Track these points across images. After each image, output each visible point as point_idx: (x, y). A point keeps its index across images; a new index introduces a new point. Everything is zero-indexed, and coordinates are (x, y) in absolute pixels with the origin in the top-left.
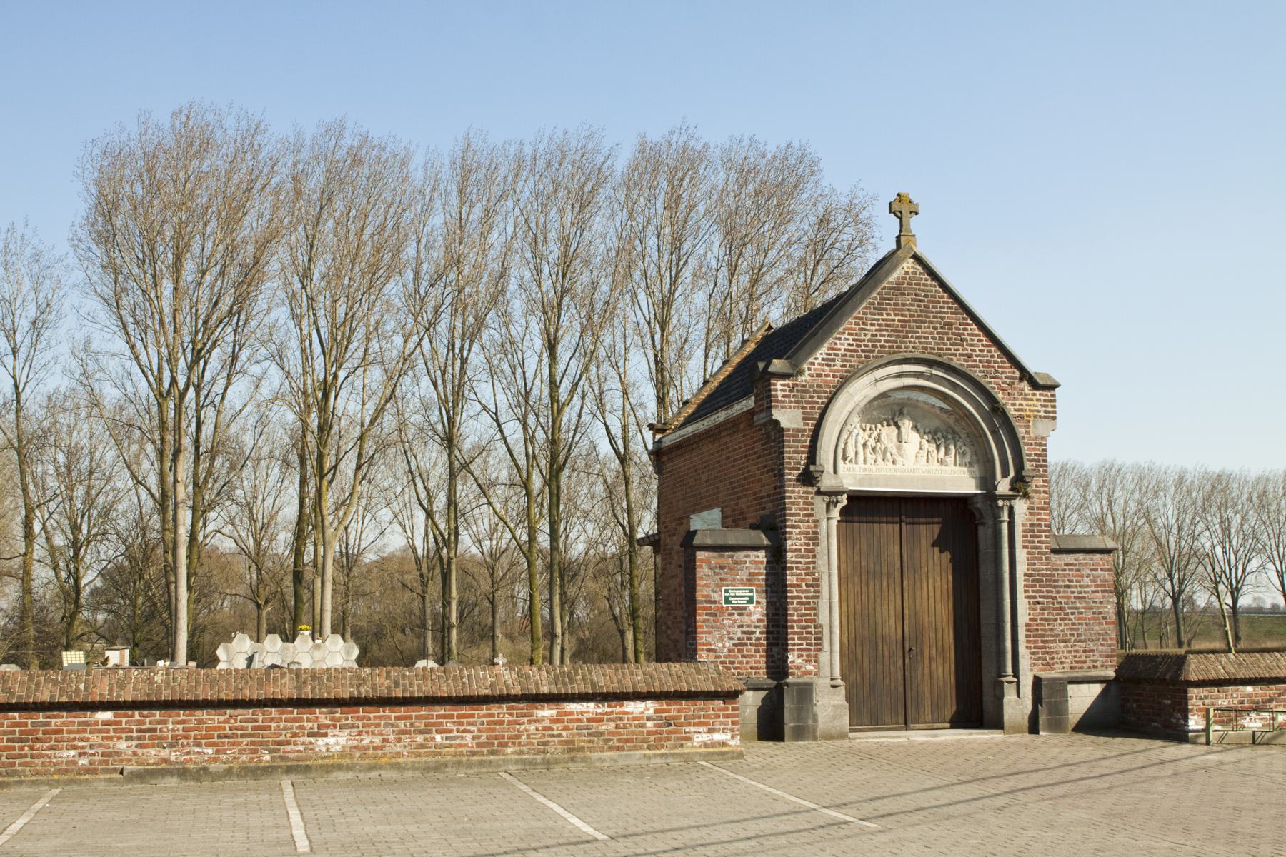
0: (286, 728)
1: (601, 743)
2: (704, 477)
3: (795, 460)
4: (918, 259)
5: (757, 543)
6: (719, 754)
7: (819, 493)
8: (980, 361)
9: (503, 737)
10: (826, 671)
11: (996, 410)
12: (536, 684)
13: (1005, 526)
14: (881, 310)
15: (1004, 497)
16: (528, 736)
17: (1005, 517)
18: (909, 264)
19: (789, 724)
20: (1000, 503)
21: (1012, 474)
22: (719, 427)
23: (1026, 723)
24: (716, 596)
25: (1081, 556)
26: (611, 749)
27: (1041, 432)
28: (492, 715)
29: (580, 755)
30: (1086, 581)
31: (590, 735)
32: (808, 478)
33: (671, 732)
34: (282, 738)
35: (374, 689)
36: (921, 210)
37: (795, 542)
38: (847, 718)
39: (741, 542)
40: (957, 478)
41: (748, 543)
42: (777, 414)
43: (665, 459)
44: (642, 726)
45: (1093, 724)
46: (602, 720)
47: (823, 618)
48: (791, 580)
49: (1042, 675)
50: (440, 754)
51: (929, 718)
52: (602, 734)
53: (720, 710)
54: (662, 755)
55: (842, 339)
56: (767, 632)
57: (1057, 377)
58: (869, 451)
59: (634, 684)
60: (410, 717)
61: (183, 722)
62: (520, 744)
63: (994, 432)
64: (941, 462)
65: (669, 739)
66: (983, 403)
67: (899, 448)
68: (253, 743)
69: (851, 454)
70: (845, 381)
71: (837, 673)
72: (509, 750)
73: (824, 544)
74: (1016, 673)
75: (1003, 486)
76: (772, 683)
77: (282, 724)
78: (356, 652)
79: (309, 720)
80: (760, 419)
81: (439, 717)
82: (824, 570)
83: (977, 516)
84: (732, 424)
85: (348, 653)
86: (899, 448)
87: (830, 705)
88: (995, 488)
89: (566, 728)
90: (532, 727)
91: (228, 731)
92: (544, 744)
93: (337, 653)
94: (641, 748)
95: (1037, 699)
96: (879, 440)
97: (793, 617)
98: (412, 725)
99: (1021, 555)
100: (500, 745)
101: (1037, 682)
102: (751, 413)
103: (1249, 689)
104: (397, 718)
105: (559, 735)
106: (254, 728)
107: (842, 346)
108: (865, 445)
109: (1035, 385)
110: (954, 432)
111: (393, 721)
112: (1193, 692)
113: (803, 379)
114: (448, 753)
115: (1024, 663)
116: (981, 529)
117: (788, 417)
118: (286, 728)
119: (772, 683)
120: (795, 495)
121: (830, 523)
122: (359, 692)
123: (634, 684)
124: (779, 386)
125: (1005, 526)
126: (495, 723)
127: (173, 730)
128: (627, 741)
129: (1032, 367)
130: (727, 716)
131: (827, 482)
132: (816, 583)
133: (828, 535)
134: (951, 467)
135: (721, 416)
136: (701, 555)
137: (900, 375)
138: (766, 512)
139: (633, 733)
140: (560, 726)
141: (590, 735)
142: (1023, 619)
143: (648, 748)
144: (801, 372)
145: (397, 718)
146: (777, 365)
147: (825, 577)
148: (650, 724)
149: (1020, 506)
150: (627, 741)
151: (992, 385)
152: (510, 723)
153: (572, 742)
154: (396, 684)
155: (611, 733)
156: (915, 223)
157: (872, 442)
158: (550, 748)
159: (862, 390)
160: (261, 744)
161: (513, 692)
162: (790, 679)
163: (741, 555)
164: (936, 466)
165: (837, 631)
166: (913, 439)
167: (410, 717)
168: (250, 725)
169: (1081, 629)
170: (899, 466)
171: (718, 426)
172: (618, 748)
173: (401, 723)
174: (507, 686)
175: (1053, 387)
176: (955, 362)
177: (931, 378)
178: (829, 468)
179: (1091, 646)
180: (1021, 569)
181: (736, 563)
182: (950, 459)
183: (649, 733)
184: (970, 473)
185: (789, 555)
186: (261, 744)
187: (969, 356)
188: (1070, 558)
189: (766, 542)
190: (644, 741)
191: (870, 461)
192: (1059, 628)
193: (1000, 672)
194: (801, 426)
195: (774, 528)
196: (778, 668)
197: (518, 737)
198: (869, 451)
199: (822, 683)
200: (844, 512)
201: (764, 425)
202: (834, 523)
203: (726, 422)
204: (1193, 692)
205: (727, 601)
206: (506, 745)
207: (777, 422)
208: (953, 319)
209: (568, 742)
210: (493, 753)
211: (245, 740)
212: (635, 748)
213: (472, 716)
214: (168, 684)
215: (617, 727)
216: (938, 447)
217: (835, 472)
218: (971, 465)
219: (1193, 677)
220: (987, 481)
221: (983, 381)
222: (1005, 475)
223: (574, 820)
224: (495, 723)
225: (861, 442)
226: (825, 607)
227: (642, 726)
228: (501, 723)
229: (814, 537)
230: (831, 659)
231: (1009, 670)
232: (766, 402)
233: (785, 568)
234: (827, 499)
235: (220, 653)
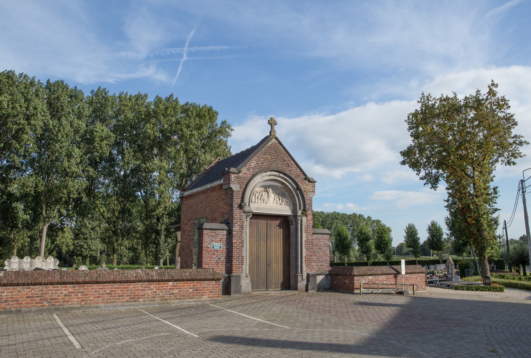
0: (55, 293)
1: (174, 297)
2: (200, 206)
3: (237, 201)
4: (277, 139)
5: (223, 228)
6: (35, 279)
7: (244, 212)
8: (294, 172)
9: (139, 295)
10: (244, 271)
11: (298, 188)
12: (151, 276)
13: (299, 225)
14: (265, 154)
15: (300, 216)
16: (148, 295)
17: (299, 222)
18: (274, 140)
19: (233, 289)
20: (298, 218)
21: (302, 208)
22: (207, 190)
23: (304, 289)
24: (209, 246)
25: (320, 235)
26: (177, 299)
27: (311, 196)
28: (135, 287)
29: (166, 302)
30: (322, 243)
31: (170, 294)
32: (241, 207)
33: (198, 293)
34: (54, 297)
35: (91, 278)
36: (278, 124)
37: (236, 228)
38: (251, 287)
39: (218, 228)
40: (285, 210)
41: (221, 228)
42: (232, 186)
43: (184, 200)
44: (188, 291)
45: (321, 288)
46: (174, 289)
47: (244, 254)
48: (234, 241)
49: (309, 272)
50: (115, 302)
51: (274, 287)
52: (174, 294)
53: (214, 285)
54: (195, 301)
55: (253, 163)
56: (226, 258)
57: (315, 179)
58: (259, 199)
59: (185, 276)
60: (105, 288)
61: (11, 292)
62: (145, 298)
63: (297, 195)
64: (280, 204)
65: (197, 295)
66: (295, 186)
67: (268, 199)
68: (41, 300)
69: (253, 200)
70: (253, 176)
71: (248, 273)
72: (141, 300)
73: (245, 229)
74: (302, 273)
75: (299, 213)
76: (227, 275)
77: (54, 292)
78: (58, 262)
79: (65, 290)
80: (225, 187)
81: (115, 288)
82: (245, 238)
83: (290, 222)
84: (213, 189)
85: (55, 262)
86: (268, 199)
87: (246, 284)
88: (297, 213)
89: (161, 292)
90: (149, 292)
91: (31, 295)
92: (153, 297)
93: (50, 264)
94: (187, 299)
95: (308, 281)
96: (262, 196)
97: (235, 253)
98: (105, 291)
99: (304, 235)
100: (137, 298)
101: (308, 275)
102: (221, 185)
103: (371, 277)
104: (99, 289)
105: (159, 294)
106: (41, 294)
107: (253, 165)
108: (258, 197)
109: (309, 181)
110: (284, 195)
111: (98, 290)
112: (356, 278)
113: (241, 174)
114: (118, 302)
115: (304, 269)
116: (291, 226)
117: (235, 187)
118: (55, 293)
119: (227, 275)
120: (237, 212)
121: (247, 223)
122: (85, 279)
123: (185, 276)
124: (233, 176)
125: (299, 225)
126: (136, 290)
127: (7, 295)
128: (183, 296)
129: (309, 176)
130: (216, 287)
131: (247, 209)
132: (242, 242)
133: (246, 226)
134: (283, 206)
135: (199, 189)
136: (205, 232)
137: (276, 176)
138: (225, 218)
139: (185, 293)
140: (159, 291)
141: (170, 294)
142: (304, 255)
143: (190, 299)
144: (240, 172)
145: (99, 289)
146: (232, 169)
147: (245, 240)
148: (190, 290)
149: (304, 219)
150: (183, 296)
151: (297, 180)
152: (141, 290)
153: (164, 297)
154: (100, 276)
155: (177, 293)
156: (276, 127)
157: (260, 197)
158: (156, 299)
159: (259, 179)
160: (45, 300)
161: (143, 279)
162: (233, 274)
163: (218, 232)
164: (279, 205)
165: (248, 258)
166: (272, 195)
167: (105, 288)
168: (40, 292)
169: (320, 258)
170: (268, 205)
171: (207, 189)
172: (179, 299)
173: (101, 291)
174: (141, 277)
175: (315, 182)
176: (287, 172)
177: (279, 177)
178: (248, 204)
179: (323, 264)
180: (304, 239)
181: (216, 235)
182: (283, 203)
183: (190, 293)
184: (290, 208)
185: (234, 232)
186: (45, 300)
187: (291, 171)
188: (317, 236)
189: (227, 228)
190: (188, 296)
191: (259, 203)
192: (314, 258)
193: (297, 272)
194: (239, 190)
195: (229, 223)
196: (229, 270)
197: (144, 295)
198: (259, 199)
199: (243, 275)
200: (251, 218)
201: (226, 189)
202: (248, 222)
203: (210, 188)
204: (356, 278)
205: (213, 248)
206: (140, 298)
207: (231, 188)
208: (286, 159)
209: (162, 297)
210: (135, 301)
211: (38, 299)
212: (185, 299)
213: (128, 288)
214: (5, 277)
215: (179, 291)
216: (280, 199)
217: (249, 206)
218: (289, 205)
219: (356, 274)
220: (294, 211)
221: (295, 179)
222: (300, 209)
223: (179, 328)
224: (136, 290)
225: (257, 196)
226: (245, 250)
227: (188, 291)
228: (138, 290)
229: (242, 227)
230: (246, 267)
231: (300, 271)
232: (228, 181)
233: (232, 237)
234: (246, 214)
235: (6, 263)
